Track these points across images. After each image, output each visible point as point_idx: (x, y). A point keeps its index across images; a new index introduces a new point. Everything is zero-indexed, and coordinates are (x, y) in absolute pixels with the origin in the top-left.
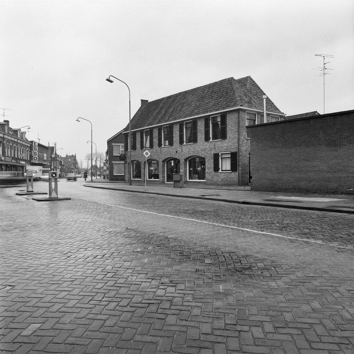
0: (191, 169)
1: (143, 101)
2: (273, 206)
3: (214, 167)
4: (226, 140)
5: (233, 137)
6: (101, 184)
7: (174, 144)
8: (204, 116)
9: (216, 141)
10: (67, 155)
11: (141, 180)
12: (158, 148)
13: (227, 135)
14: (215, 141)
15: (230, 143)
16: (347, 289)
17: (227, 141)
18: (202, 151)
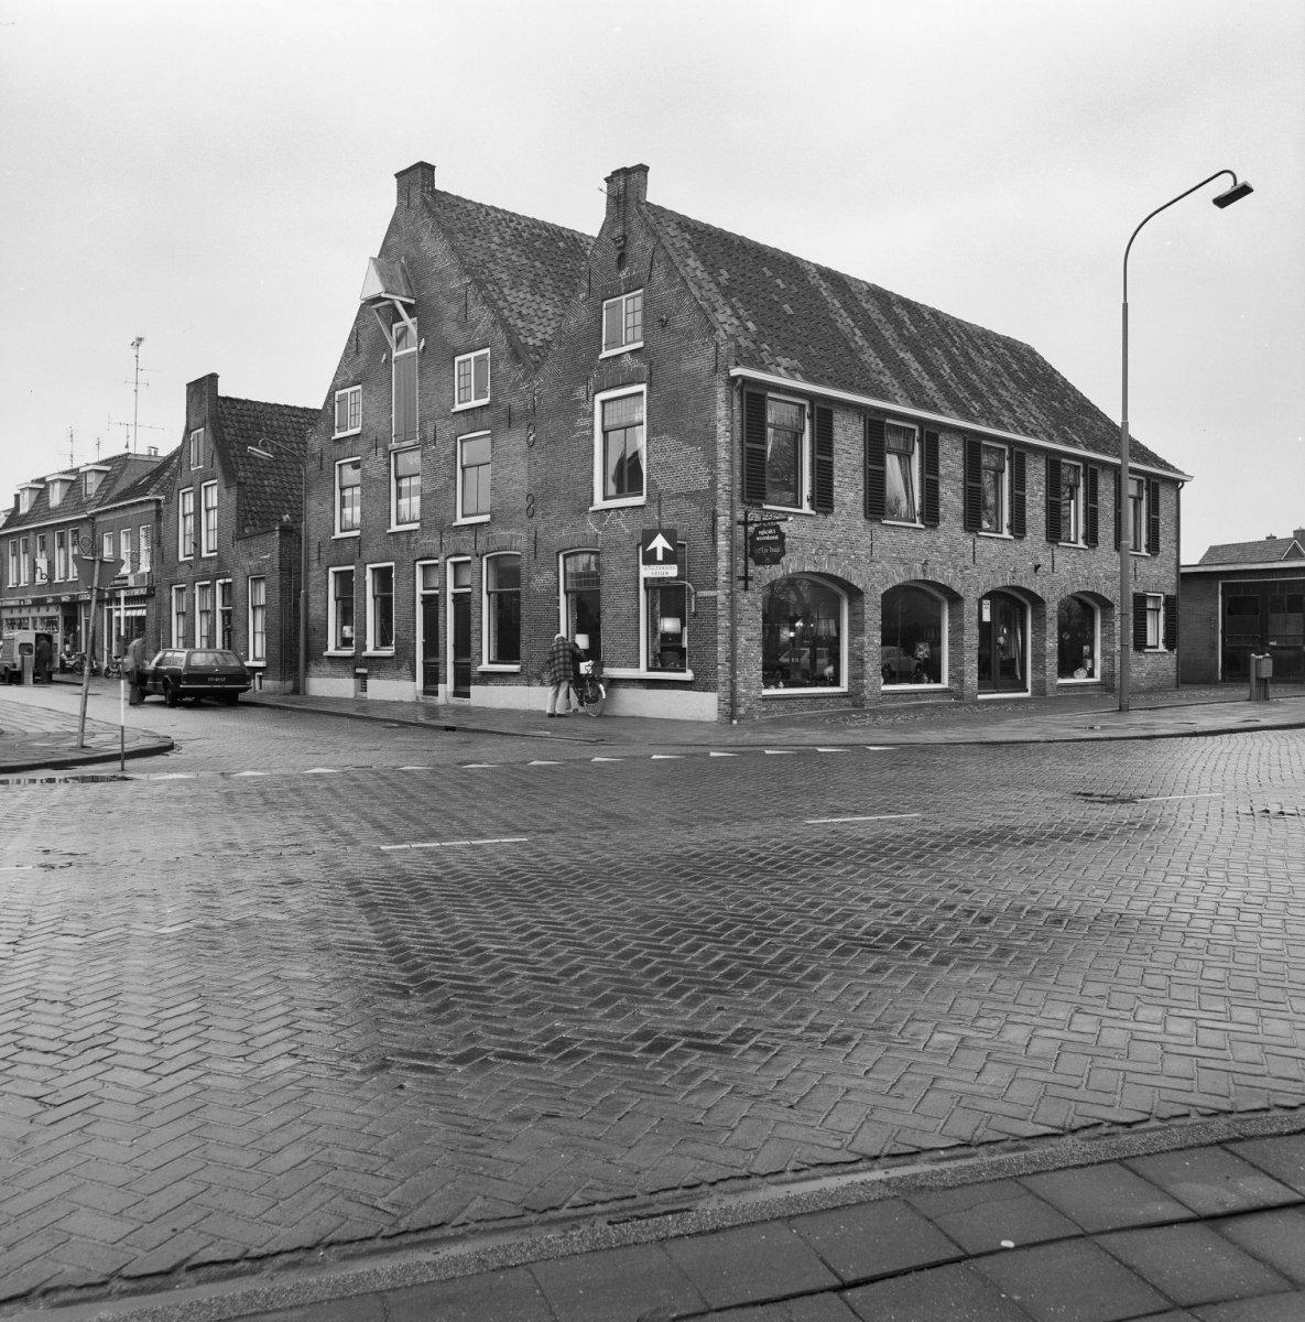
1: (416, 180)
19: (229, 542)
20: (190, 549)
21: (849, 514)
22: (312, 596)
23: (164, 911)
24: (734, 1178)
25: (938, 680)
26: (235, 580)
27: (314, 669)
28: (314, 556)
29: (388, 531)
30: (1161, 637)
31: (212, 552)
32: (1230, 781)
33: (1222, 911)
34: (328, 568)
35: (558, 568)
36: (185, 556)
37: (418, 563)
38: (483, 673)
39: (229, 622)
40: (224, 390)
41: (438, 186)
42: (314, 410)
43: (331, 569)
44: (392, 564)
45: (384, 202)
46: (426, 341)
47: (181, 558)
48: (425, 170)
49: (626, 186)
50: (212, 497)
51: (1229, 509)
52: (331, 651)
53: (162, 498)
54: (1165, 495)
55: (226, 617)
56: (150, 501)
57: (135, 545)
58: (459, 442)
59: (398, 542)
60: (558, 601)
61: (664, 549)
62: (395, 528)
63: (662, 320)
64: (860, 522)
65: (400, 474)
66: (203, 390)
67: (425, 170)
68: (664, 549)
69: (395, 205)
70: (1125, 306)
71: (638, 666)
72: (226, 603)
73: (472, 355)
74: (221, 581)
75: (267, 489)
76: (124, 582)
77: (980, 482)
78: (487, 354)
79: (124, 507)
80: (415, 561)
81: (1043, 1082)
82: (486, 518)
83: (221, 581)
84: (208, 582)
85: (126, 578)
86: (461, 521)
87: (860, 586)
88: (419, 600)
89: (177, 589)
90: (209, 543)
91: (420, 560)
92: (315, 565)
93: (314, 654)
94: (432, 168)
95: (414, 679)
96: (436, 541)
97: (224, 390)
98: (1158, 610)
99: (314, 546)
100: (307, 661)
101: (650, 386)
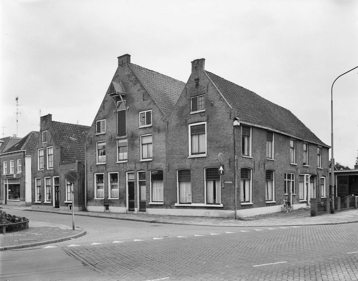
19: (58, 165)
20: (42, 166)
22: (89, 182)
23: (302, 275)
26: (60, 177)
27: (89, 203)
28: (89, 169)
29: (116, 163)
31: (41, 169)
33: (319, 270)
34: (94, 173)
35: (176, 174)
36: (40, 169)
37: (127, 172)
38: (151, 205)
39: (58, 189)
40: (53, 119)
41: (131, 62)
42: (89, 127)
43: (95, 174)
44: (118, 172)
45: (114, 66)
46: (129, 107)
47: (39, 170)
48: (128, 56)
49: (198, 64)
50: (51, 151)
52: (95, 198)
53: (25, 151)
55: (56, 188)
56: (22, 151)
57: (15, 165)
58: (141, 137)
59: (97, 166)
60: (177, 184)
61: (222, 170)
62: (118, 162)
63: (212, 104)
65: (119, 146)
66: (46, 119)
67: (128, 56)
68: (222, 170)
69: (191, 73)
70: (332, 101)
71: (204, 203)
72: (56, 184)
73: (145, 112)
74: (55, 177)
75: (68, 149)
76: (12, 176)
78: (151, 112)
79: (12, 153)
80: (126, 172)
82: (151, 160)
83: (55, 177)
84: (50, 177)
85: (13, 175)
86: (142, 160)
88: (127, 183)
89: (46, 178)
90: (50, 165)
91: (127, 171)
92: (90, 172)
93: (90, 199)
94: (130, 56)
95: (126, 206)
96: (133, 166)
97: (53, 119)
99: (89, 167)
100: (87, 201)
101: (208, 122)
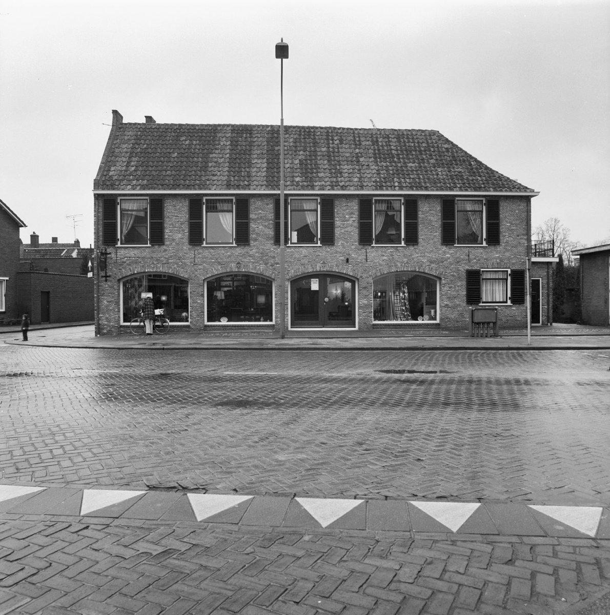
0: (261, 299)
1: (146, 117)
2: (502, 348)
3: (469, 291)
4: (498, 246)
5: (515, 243)
6: (173, 344)
7: (339, 243)
8: (358, 195)
9: (472, 247)
10: (34, 233)
11: (188, 327)
12: (269, 246)
13: (501, 238)
14: (469, 247)
15: (507, 254)
16: (78, 521)
17: (499, 248)
18: (431, 262)
21: (178, 244)
24: (365, 583)
25: (271, 320)
30: (509, 295)
32: (566, 378)
51: (569, 218)
54: (507, 215)
64: (186, 247)
77: (105, 223)
81: (471, 549)
87: (186, 276)
98: (507, 280)
